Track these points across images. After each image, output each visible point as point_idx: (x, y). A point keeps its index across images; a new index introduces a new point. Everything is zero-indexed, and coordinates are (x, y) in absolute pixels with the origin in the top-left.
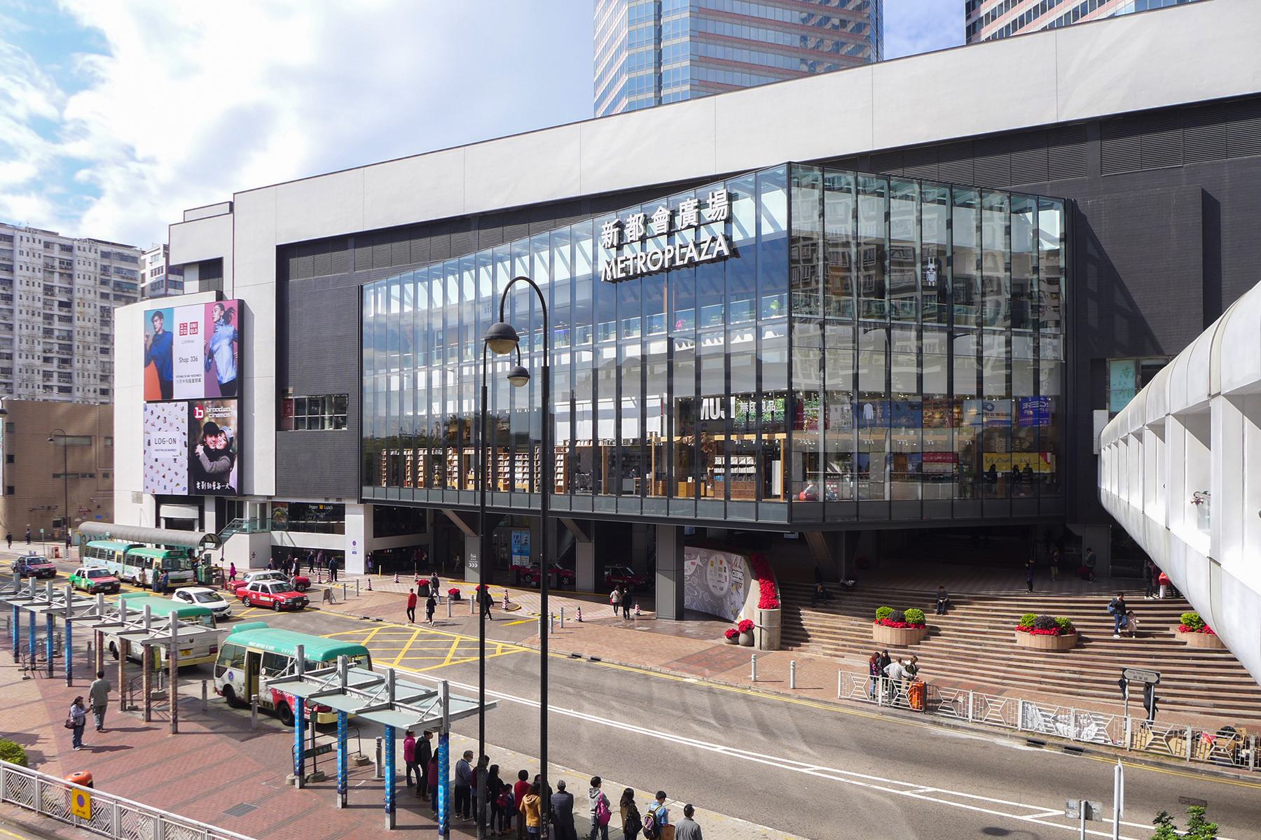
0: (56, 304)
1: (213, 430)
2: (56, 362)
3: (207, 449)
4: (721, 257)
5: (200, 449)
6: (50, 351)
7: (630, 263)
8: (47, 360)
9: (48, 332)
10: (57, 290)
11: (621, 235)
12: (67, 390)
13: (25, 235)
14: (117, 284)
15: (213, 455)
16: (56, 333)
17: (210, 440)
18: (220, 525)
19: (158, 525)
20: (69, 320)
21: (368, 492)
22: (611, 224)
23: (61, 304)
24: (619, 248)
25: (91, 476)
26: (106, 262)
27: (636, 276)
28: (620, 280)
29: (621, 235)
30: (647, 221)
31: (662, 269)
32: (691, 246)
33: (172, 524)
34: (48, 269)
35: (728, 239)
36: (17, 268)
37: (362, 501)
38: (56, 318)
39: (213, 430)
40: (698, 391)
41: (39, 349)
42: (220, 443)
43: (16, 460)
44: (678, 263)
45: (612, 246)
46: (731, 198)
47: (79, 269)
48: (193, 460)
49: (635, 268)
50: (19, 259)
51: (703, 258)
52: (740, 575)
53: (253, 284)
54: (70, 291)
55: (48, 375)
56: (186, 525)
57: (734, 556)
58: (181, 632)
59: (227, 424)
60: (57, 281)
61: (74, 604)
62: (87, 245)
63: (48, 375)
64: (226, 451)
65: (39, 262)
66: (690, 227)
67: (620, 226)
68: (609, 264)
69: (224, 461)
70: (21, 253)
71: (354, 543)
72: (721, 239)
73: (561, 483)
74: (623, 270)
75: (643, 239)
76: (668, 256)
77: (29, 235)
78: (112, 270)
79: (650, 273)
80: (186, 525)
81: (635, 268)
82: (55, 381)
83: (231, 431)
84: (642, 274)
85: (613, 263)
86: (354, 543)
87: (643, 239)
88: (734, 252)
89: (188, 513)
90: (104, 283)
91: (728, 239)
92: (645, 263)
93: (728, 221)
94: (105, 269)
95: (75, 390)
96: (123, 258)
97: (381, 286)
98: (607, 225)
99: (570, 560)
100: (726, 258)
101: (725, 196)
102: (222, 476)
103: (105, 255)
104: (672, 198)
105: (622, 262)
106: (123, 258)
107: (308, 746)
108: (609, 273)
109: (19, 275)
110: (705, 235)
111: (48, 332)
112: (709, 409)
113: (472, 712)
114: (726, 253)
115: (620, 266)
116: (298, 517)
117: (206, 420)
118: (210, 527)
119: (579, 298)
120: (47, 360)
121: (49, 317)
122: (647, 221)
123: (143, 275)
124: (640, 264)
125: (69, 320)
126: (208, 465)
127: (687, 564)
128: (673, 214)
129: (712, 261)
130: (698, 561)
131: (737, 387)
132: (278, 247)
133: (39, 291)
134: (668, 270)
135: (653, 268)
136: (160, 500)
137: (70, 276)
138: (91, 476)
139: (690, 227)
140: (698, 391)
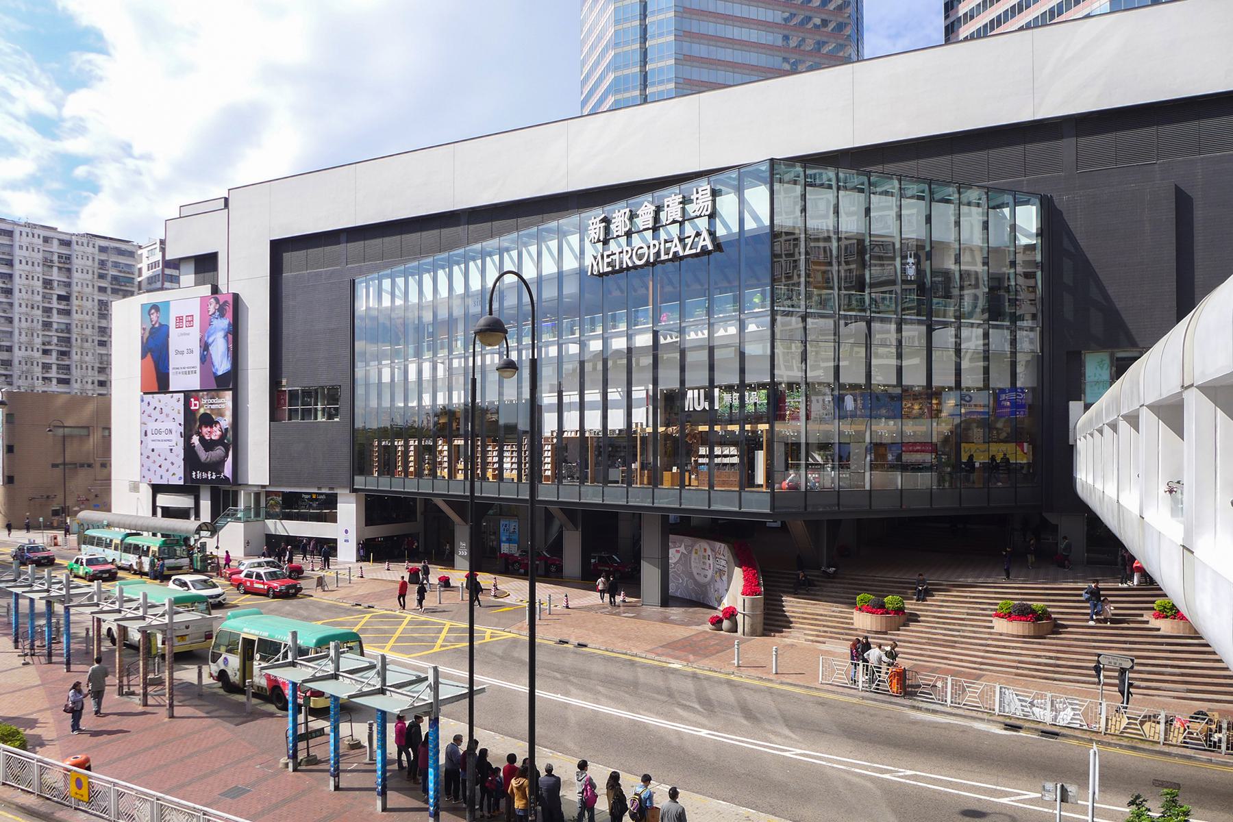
0: (55, 297)
1: (208, 420)
2: (54, 354)
3: (202, 440)
4: (705, 252)
5: (195, 440)
6: (49, 343)
7: (616, 257)
8: (46, 352)
9: (47, 325)
10: (55, 284)
11: (607, 230)
12: (66, 382)
13: (25, 230)
14: (115, 278)
15: (208, 445)
16: (55, 326)
17: (205, 430)
18: (215, 513)
19: (154, 513)
20: (67, 313)
21: (360, 481)
22: (598, 219)
23: (60, 298)
24: (606, 242)
25: (89, 466)
26: (103, 257)
27: (621, 270)
28: (607, 274)
29: (607, 230)
30: (632, 216)
31: (648, 263)
32: (676, 241)
33: (168, 512)
34: (47, 263)
35: (712, 234)
36: (16, 262)
37: (354, 491)
38: (55, 311)
39: (208, 420)
40: (682, 382)
41: (38, 341)
42: (215, 434)
43: (15, 450)
44: (663, 257)
45: (599, 241)
46: (715, 193)
47: (77, 263)
48: (189, 450)
49: (621, 263)
50: (19, 254)
51: (688, 252)
52: (723, 563)
53: (248, 278)
54: (68, 285)
55: (47, 367)
56: (182, 514)
57: (718, 545)
58: (177, 619)
59: (222, 415)
60: (55, 275)
61: (73, 591)
62: (85, 240)
63: (47, 367)
64: (221, 441)
65: (39, 257)
66: (674, 222)
67: (607, 221)
68: (595, 258)
69: (219, 451)
70: (21, 247)
71: (346, 532)
72: (705, 234)
73: (548, 473)
74: (609, 264)
75: (629, 234)
76: (653, 251)
77: (28, 230)
78: (109, 264)
79: (635, 267)
80: (182, 514)
81: (621, 263)
82: (53, 373)
83: (226, 422)
84: (628, 268)
85: (599, 257)
86: (346, 532)
87: (629, 234)
88: (718, 246)
89: (184, 502)
90: (101, 276)
91: (712, 234)
92: (631, 258)
93: (712, 216)
94: (102, 263)
95: (73, 381)
96: (120, 252)
97: (373, 279)
98: (593, 220)
99: (557, 548)
100: (709, 252)
101: (708, 191)
102: (217, 466)
103: (103, 250)
104: (658, 194)
105: (608, 256)
106: (120, 252)
107: (302, 730)
108: (595, 267)
109: (19, 269)
110: (689, 230)
111: (47, 325)
112: (694, 400)
113: (461, 697)
114: (710, 247)
115: (606, 261)
116: (292, 506)
117: (202, 411)
118: (206, 516)
119: (566, 291)
120: (46, 352)
121: (48, 311)
122: (632, 216)
123: (140, 270)
124: (626, 258)
125: (67, 313)
126: (203, 455)
127: (672, 552)
128: (658, 210)
129: (696, 255)
130: (682, 549)
131: (720, 379)
132: (272, 242)
133: (38, 285)
134: (654, 264)
135: (638, 263)
136: (157, 489)
137: (69, 270)
138: (89, 466)
139: (674, 222)
140: (682, 382)
